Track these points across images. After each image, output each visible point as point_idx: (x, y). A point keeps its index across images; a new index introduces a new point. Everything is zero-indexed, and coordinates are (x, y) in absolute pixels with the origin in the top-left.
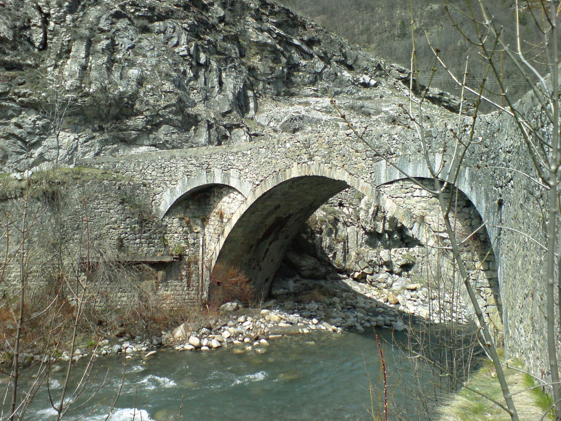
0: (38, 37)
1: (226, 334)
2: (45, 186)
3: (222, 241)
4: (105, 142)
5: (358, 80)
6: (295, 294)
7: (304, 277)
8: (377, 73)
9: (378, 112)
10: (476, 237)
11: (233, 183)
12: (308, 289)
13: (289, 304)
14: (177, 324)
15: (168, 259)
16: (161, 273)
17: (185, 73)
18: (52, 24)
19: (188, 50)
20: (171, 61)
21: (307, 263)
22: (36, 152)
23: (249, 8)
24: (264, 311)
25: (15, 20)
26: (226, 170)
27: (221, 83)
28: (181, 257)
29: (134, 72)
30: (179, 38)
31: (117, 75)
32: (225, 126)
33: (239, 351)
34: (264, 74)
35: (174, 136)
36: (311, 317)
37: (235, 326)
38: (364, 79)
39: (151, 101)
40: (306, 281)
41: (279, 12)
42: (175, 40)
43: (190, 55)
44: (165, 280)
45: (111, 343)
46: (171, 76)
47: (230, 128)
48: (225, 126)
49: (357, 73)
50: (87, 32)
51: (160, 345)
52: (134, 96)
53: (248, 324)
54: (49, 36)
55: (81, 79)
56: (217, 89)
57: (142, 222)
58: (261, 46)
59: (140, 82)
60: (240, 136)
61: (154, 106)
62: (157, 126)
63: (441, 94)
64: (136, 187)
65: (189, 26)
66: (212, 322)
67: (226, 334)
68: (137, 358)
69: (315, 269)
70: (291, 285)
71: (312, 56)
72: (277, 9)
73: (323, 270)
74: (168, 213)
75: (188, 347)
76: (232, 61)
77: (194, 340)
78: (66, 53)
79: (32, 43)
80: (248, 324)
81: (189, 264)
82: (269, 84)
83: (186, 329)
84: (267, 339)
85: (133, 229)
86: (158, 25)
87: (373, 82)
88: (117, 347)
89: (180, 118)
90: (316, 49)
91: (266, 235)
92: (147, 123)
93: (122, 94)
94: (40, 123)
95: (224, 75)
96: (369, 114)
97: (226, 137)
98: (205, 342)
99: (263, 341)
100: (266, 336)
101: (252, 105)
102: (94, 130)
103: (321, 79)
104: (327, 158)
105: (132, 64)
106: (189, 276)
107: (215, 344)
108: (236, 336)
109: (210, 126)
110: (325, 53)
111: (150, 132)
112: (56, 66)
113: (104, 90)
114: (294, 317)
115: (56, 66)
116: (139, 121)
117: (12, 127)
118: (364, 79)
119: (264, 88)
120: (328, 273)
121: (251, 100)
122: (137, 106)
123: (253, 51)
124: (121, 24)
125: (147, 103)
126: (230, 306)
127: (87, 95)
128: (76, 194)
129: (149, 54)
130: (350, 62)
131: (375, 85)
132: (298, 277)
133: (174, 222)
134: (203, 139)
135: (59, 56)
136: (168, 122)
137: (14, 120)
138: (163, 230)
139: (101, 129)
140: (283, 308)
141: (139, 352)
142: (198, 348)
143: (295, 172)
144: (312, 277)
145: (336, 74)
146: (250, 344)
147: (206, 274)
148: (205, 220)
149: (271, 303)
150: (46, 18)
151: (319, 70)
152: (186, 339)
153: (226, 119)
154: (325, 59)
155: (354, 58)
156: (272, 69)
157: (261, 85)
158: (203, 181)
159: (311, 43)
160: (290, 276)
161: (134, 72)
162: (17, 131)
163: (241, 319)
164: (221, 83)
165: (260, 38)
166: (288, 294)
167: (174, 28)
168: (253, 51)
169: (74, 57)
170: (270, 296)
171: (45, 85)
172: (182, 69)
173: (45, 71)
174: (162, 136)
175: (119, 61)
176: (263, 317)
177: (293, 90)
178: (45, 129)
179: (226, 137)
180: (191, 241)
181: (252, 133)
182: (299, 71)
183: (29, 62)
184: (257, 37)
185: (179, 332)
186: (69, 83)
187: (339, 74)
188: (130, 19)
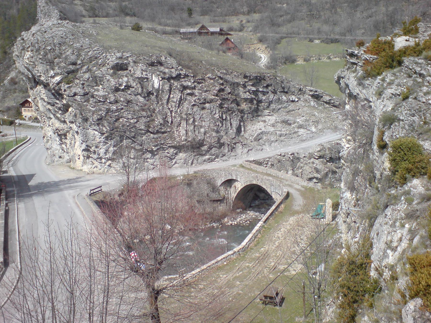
0: (170, 120)
1: (238, 220)
2: (187, 181)
3: (236, 194)
4: (195, 156)
5: (290, 99)
6: (258, 205)
7: (261, 200)
8: (299, 93)
9: (294, 123)
10: (425, 115)
11: (239, 180)
12: (262, 204)
13: (256, 209)
14: (225, 217)
15: (221, 199)
16: (219, 202)
17: (219, 125)
18: (173, 114)
19: (219, 115)
20: (213, 122)
21: (262, 195)
22: (174, 161)
23: (240, 84)
24: (248, 212)
25: (163, 116)
26: (236, 175)
27: (231, 124)
28: (224, 198)
29: (202, 130)
30: (216, 111)
31: (197, 132)
32: (233, 144)
33: (242, 225)
34: (247, 111)
35: (217, 151)
36: (262, 214)
37: (240, 217)
38: (292, 99)
39: (209, 141)
40: (261, 201)
41: (253, 79)
42: (214, 112)
43: (220, 117)
44: (220, 204)
45: (210, 223)
46: (214, 130)
47: (235, 144)
48: (233, 144)
49: (290, 95)
50: (185, 117)
51: (222, 224)
52: (204, 140)
53: (244, 217)
54: (173, 119)
55: (186, 136)
56: (230, 128)
57: (213, 189)
58: (246, 100)
59: (205, 133)
60: (239, 146)
61: (210, 143)
62: (212, 148)
63: (330, 100)
64: (211, 179)
65: (219, 105)
66: (234, 216)
67: (238, 220)
68: (218, 227)
69: (264, 197)
70: (257, 202)
71: (268, 92)
72: (252, 78)
73: (267, 197)
74: (220, 186)
75: (229, 224)
76: (235, 112)
77: (231, 222)
78: (179, 125)
79: (168, 122)
80: (244, 217)
81: (226, 199)
82: (249, 114)
83: (228, 219)
84: (249, 221)
85: (211, 191)
86: (207, 105)
87: (296, 100)
88: (212, 225)
89: (219, 145)
90: (270, 88)
91: (248, 191)
92: (208, 148)
93: (200, 140)
94: (175, 152)
95: (232, 120)
96: (290, 124)
97: (234, 148)
98: (233, 223)
99: (248, 222)
100: (249, 220)
101: (243, 129)
102: (191, 152)
103: (272, 103)
104: (261, 182)
105: (201, 127)
106: (226, 203)
107: (236, 223)
108: (241, 220)
109: (229, 145)
110: (274, 90)
111: (209, 151)
112: (177, 131)
113: (194, 139)
114: (257, 214)
115: (177, 131)
116: (205, 148)
117: (166, 153)
118: (292, 99)
119: (247, 116)
120: (269, 198)
121: (242, 127)
122: (205, 143)
123: (242, 101)
124: (195, 109)
125: (208, 142)
126: (238, 211)
127: (189, 141)
128: (195, 182)
129: (206, 120)
130: (286, 90)
131: (297, 101)
132: (259, 200)
133: (222, 188)
134: (226, 151)
135: (177, 127)
136: (215, 147)
137: (166, 151)
138: (218, 190)
139: (194, 152)
140: (254, 211)
141: (217, 226)
142: (232, 224)
143: (254, 182)
144: (263, 200)
145: (279, 99)
146: (245, 223)
147: (232, 202)
148: (231, 187)
149: (251, 209)
150: (171, 112)
151: (271, 100)
152: (228, 222)
153: (234, 140)
154: (275, 92)
155: (288, 88)
156: (250, 108)
157: (246, 116)
158: (230, 178)
159: (267, 86)
160: (256, 200)
161: (202, 130)
162: (168, 155)
163: (242, 215)
164: (231, 124)
165: (245, 96)
166: (256, 206)
167: (214, 107)
168: (242, 101)
169: (182, 127)
170: (250, 207)
171: (175, 139)
172: (218, 124)
173: (174, 132)
174: (213, 152)
175: (197, 126)
176: (248, 214)
177: (260, 113)
178: (176, 154)
179: (234, 148)
180: (227, 193)
181: (243, 144)
182: (262, 102)
183: (168, 130)
184: (244, 96)
185: (226, 220)
186: (183, 138)
187: (281, 98)
188: (198, 106)
